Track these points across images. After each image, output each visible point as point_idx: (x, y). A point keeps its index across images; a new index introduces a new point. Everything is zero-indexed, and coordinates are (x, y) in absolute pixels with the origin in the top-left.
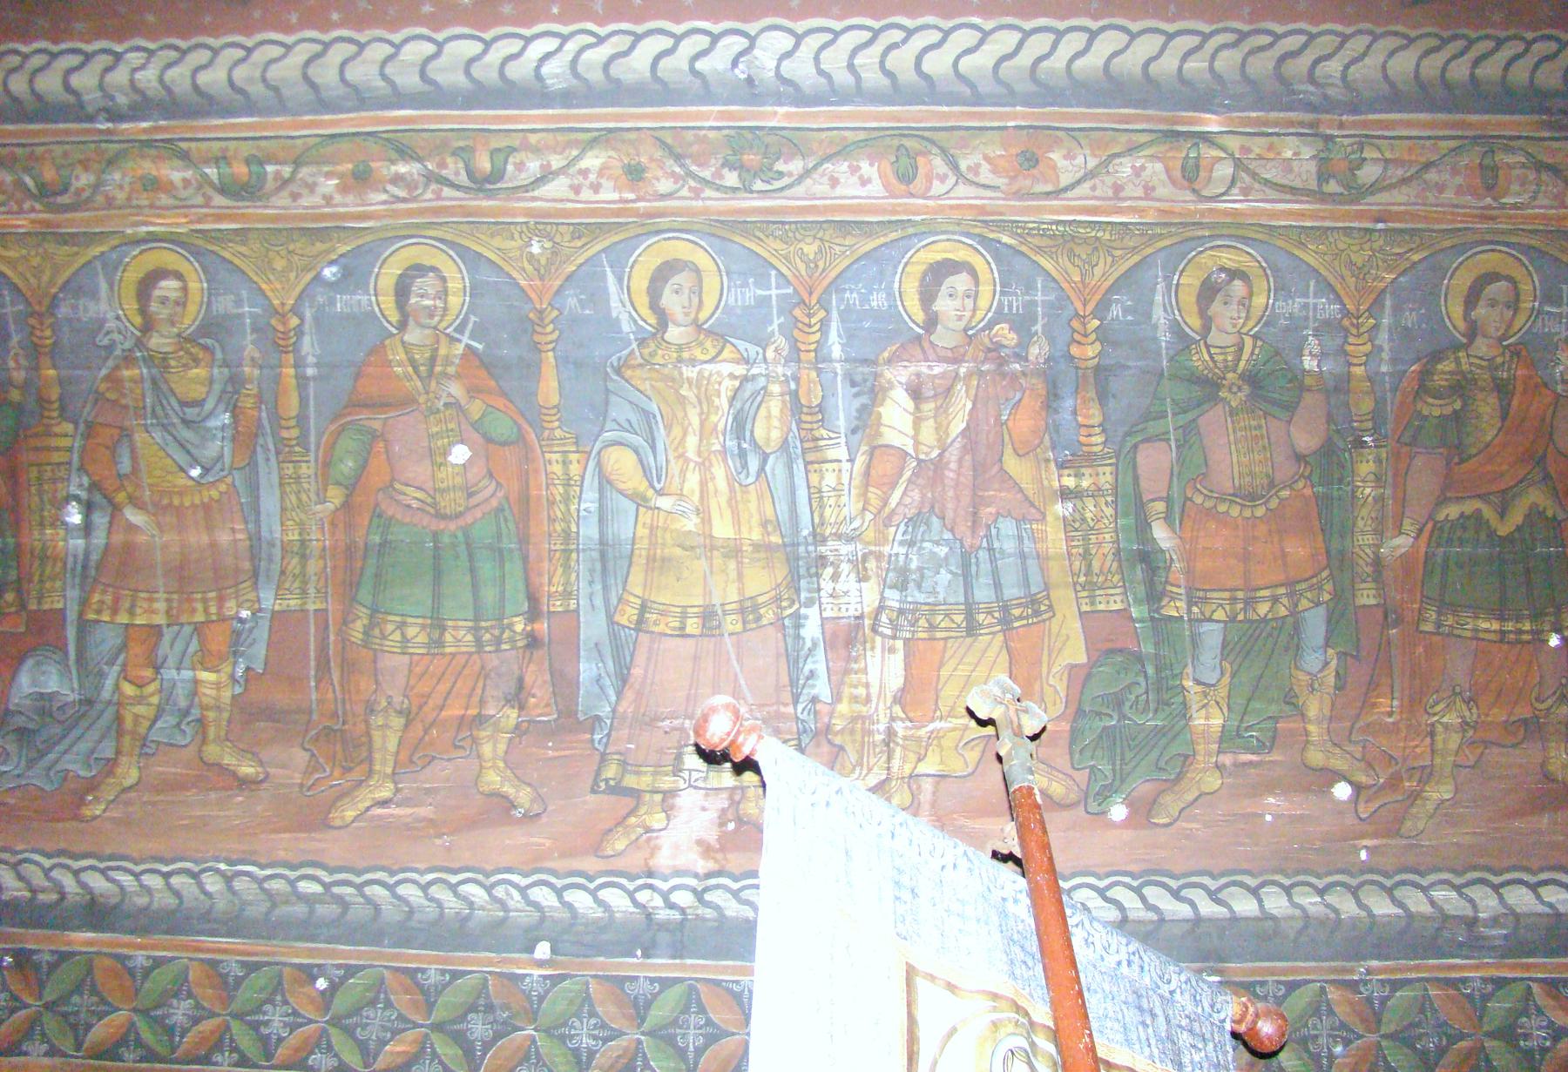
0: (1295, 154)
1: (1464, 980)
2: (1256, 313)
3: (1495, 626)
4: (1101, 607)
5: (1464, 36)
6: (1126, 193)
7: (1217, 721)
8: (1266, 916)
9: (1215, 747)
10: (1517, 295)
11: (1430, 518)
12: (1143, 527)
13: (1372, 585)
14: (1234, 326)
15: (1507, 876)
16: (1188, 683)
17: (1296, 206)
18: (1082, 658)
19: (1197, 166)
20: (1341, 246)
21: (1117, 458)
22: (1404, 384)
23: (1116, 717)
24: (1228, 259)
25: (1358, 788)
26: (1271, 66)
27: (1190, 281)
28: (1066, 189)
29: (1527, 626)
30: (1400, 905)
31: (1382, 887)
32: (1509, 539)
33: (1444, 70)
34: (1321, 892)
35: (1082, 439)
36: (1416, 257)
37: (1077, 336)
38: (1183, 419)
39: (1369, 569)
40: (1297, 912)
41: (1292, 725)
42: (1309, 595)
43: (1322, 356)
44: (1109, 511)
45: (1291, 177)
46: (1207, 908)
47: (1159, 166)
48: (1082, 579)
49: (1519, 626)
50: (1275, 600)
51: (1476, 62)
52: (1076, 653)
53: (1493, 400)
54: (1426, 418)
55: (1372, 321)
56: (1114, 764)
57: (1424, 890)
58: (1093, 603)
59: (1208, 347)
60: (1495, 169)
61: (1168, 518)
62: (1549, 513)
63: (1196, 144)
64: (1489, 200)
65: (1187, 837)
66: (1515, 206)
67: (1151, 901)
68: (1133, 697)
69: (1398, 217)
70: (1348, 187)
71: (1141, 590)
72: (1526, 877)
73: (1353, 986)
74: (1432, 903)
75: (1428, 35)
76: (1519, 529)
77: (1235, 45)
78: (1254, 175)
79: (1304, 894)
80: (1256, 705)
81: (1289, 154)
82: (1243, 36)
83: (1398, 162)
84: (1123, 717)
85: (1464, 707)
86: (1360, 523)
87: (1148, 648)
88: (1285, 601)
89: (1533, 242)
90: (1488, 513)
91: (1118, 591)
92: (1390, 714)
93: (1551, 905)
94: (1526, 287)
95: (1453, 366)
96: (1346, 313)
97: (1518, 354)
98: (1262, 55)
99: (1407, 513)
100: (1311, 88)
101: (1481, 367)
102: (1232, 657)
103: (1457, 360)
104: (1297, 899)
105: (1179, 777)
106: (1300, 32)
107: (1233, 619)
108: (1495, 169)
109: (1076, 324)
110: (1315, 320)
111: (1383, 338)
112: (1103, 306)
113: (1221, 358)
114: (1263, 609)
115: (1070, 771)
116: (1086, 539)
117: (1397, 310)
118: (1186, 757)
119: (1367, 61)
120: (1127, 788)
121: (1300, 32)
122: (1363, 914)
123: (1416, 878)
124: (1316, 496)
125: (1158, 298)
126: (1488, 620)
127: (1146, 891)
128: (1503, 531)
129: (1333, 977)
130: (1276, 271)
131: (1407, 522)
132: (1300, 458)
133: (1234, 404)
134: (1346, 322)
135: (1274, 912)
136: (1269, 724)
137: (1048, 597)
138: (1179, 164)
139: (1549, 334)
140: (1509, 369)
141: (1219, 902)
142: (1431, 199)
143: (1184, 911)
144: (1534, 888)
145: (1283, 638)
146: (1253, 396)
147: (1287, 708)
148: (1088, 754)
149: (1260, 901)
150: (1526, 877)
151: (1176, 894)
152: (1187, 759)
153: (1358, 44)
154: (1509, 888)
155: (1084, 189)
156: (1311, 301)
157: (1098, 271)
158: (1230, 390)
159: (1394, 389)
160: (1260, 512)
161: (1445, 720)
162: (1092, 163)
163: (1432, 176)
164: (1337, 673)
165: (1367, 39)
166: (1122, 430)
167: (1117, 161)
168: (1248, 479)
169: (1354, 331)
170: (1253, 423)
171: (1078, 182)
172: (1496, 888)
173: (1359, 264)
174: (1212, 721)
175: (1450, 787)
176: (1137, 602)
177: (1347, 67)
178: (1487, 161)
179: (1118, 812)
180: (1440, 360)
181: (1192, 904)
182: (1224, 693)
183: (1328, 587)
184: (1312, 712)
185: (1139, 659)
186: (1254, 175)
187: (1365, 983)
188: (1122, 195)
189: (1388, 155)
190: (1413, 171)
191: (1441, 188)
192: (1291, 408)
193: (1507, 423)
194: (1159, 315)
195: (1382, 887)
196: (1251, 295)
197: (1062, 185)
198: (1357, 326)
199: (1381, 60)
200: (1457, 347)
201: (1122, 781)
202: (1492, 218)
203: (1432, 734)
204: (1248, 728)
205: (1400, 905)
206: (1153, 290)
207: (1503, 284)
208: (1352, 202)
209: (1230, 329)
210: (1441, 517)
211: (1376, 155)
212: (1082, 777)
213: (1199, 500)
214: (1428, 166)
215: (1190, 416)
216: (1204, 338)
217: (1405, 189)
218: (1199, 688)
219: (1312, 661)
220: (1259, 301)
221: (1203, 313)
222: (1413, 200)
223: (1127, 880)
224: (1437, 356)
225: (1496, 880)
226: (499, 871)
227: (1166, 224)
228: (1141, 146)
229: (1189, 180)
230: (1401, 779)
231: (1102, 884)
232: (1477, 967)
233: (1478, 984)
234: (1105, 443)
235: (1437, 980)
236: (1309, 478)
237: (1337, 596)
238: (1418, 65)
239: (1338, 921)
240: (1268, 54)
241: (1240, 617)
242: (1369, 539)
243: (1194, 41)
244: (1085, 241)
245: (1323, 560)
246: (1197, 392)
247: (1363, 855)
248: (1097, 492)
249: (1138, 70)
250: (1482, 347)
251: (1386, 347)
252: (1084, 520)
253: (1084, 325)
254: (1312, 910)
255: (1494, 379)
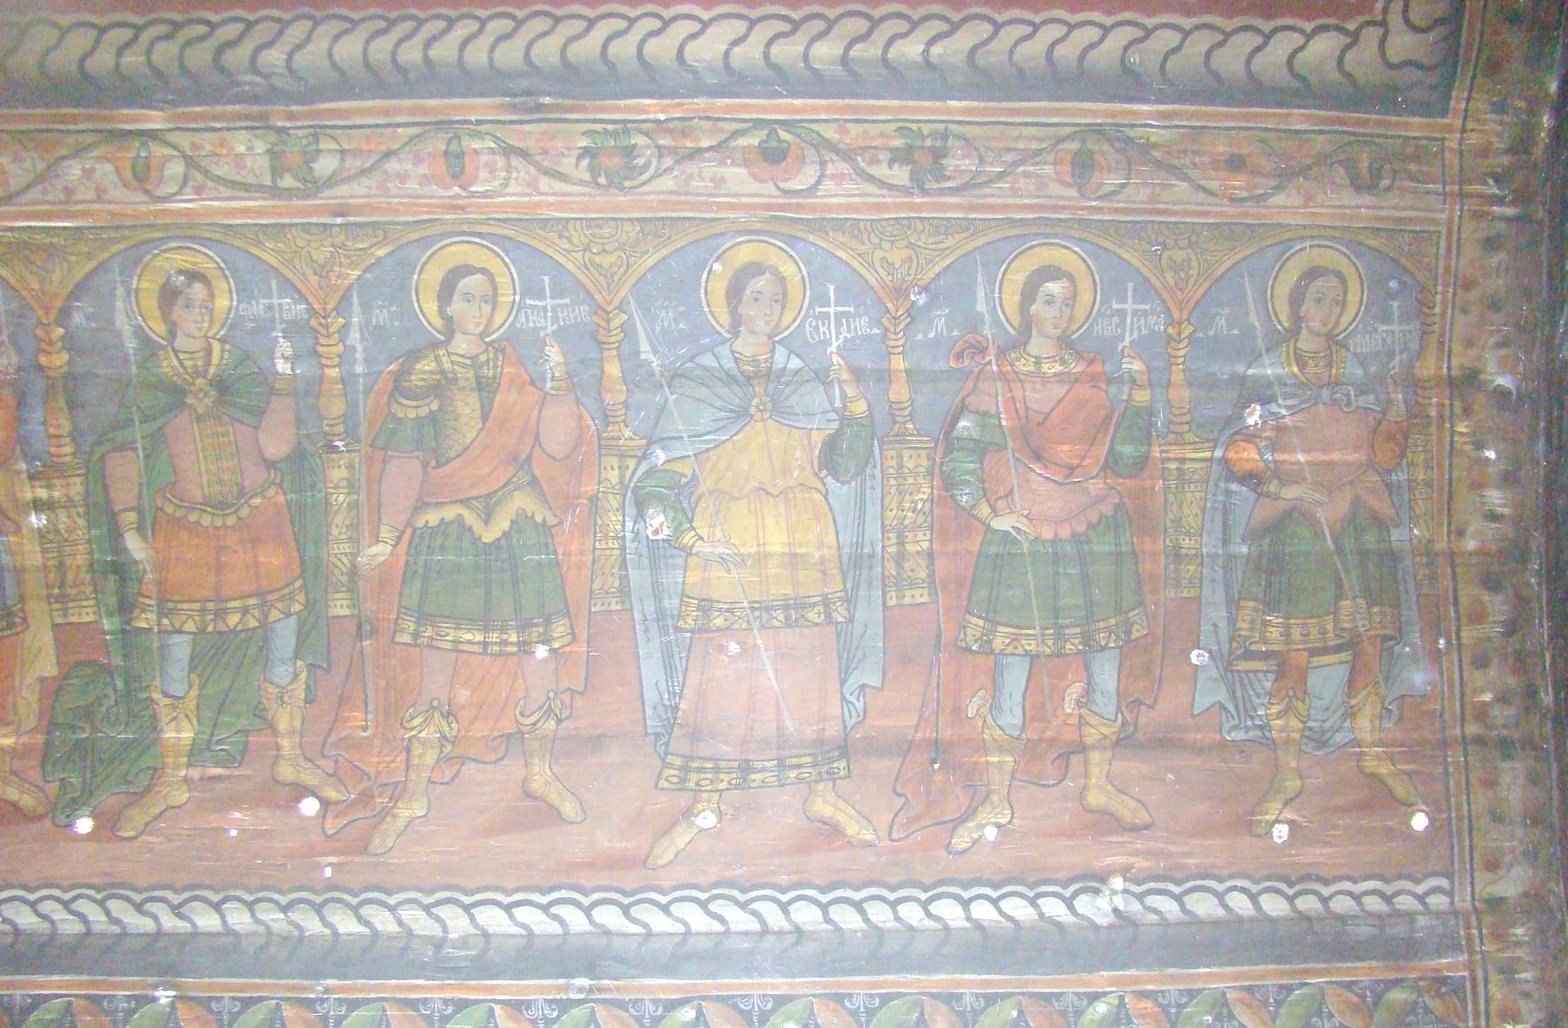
0: (249, 149)
1: (425, 1001)
2: (220, 315)
3: (479, 637)
4: (73, 619)
5: (413, 18)
6: (79, 196)
7: (187, 735)
8: (229, 931)
9: (185, 760)
10: (495, 289)
11: (409, 523)
12: (116, 534)
13: (348, 595)
14: (200, 329)
15: (479, 897)
16: (156, 696)
17: (251, 204)
18: (52, 671)
19: (148, 167)
20: (300, 243)
21: (87, 467)
22: (379, 385)
23: (88, 729)
24: (181, 260)
25: (325, 803)
26: (209, 57)
27: (149, 286)
28: (18, 194)
29: (513, 638)
30: (367, 924)
31: (348, 905)
32: (496, 544)
33: (394, 54)
34: (285, 909)
35: (53, 450)
36: (381, 253)
37: (44, 346)
38: (151, 427)
39: (344, 579)
40: (261, 929)
41: (262, 739)
42: (280, 606)
43: (294, 359)
44: (81, 522)
45: (243, 173)
46: (170, 923)
47: (109, 167)
48: (56, 591)
49: (505, 637)
50: (245, 611)
51: (428, 45)
52: (48, 666)
53: (474, 399)
54: (400, 421)
55: (341, 320)
56: (84, 776)
57: (392, 909)
58: (65, 616)
59: (176, 352)
60: (460, 156)
61: (140, 529)
62: (539, 519)
63: (144, 144)
64: (457, 189)
65: (151, 850)
66: (484, 195)
67: (115, 914)
68: (103, 709)
69: (359, 210)
70: (304, 181)
71: (113, 601)
72: (500, 897)
73: (309, 1004)
74: (400, 923)
75: (371, 18)
76: (506, 535)
77: (168, 37)
78: (206, 173)
79: (267, 911)
80: (225, 718)
81: (241, 149)
82: (176, 27)
83: (356, 153)
84: (95, 729)
85: (444, 723)
86: (335, 531)
87: (117, 660)
88: (256, 612)
89: (505, 232)
90: (470, 519)
91: (92, 602)
92: (365, 729)
93: (524, 926)
94: (502, 280)
95: (433, 366)
96: (312, 312)
97: (503, 351)
98: (197, 46)
99: (384, 520)
100: (257, 79)
101: (464, 366)
102: (199, 670)
103: (437, 359)
104: (260, 916)
105: (148, 790)
106: (237, 20)
107: (202, 631)
108: (460, 156)
109: (40, 333)
110: (282, 321)
111: (354, 337)
112: (64, 314)
113: (191, 363)
114: (233, 620)
115: (41, 783)
116: (60, 550)
117: (366, 307)
118: (156, 769)
119: (310, 47)
120: (94, 802)
121: (237, 20)
122: (327, 931)
123: (382, 896)
124: (288, 504)
125: (119, 304)
126: (469, 630)
127: (112, 904)
128: (488, 537)
129: (289, 995)
130: (234, 271)
131: (383, 529)
132: (270, 465)
133: (200, 411)
134: (314, 323)
135: (237, 928)
136: (238, 738)
137: (23, 610)
138: (128, 164)
139: (535, 328)
140: (495, 366)
141: (180, 916)
142: (394, 191)
143: (148, 925)
144: (508, 908)
145: (253, 650)
146: (219, 401)
147: (257, 721)
148: (59, 766)
149: (223, 917)
150: (500, 897)
151: (139, 908)
152: (156, 772)
153: (298, 30)
154: (9, 905)
155: (35, 193)
156: (276, 301)
157: (56, 277)
158: (197, 397)
159: (367, 392)
160: (231, 520)
161: (423, 735)
162: (41, 166)
163: (392, 166)
164: (308, 686)
165: (307, 24)
166: (90, 439)
167: (66, 163)
168: (217, 488)
169: (323, 331)
170: (220, 430)
171: (28, 187)
172: (467, 908)
173: (321, 261)
174: (183, 735)
175: (425, 805)
176: (110, 615)
177: (290, 55)
178: (454, 147)
179: (84, 825)
180: (417, 360)
181: (155, 918)
182: (192, 705)
183: (301, 598)
184: (283, 725)
185: (110, 671)
186: (206, 173)
187: (322, 1001)
188: (74, 198)
189: (346, 146)
190: (373, 160)
191: (403, 177)
192: (258, 412)
193: (490, 423)
194: (122, 323)
195: (348, 905)
196: (212, 296)
197: (13, 189)
198: (327, 326)
199: (326, 46)
200: (435, 345)
201: (91, 793)
202: (463, 208)
203: (408, 750)
204: (218, 742)
205: (367, 924)
206: (113, 296)
207: (1065, 283)
208: (309, 197)
209: (196, 333)
210: (420, 523)
211: (334, 146)
212: (53, 789)
213: (169, 509)
214: (389, 154)
215: (155, 425)
216: (172, 344)
217: (364, 181)
218: (167, 701)
219: (281, 674)
220: (222, 303)
221: (166, 316)
222: (374, 191)
223: (91, 892)
224: (415, 355)
225: (467, 900)
226: (367, 889)
227: (117, 228)
228: (87, 148)
229: (140, 181)
230: (373, 797)
231: (67, 896)
232: (441, 988)
233: (438, 1005)
234: (74, 454)
235: (397, 1000)
236: (280, 485)
237: (309, 605)
238: (365, 50)
239: (301, 938)
240: (206, 44)
241: (210, 629)
242: (347, 548)
243: (127, 34)
244: (40, 247)
245: (296, 567)
246: (163, 399)
247: (328, 872)
248: (69, 504)
249: (74, 68)
250: (461, 345)
251: (359, 347)
252: (57, 531)
253: (48, 333)
254: (276, 927)
255: (478, 378)
